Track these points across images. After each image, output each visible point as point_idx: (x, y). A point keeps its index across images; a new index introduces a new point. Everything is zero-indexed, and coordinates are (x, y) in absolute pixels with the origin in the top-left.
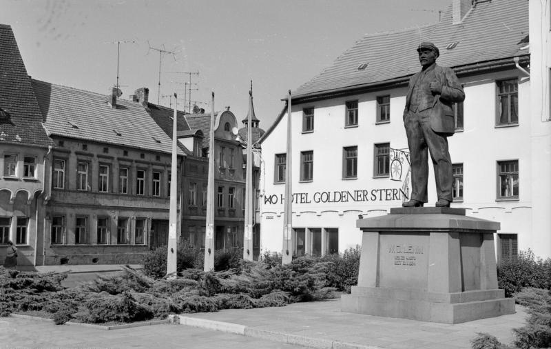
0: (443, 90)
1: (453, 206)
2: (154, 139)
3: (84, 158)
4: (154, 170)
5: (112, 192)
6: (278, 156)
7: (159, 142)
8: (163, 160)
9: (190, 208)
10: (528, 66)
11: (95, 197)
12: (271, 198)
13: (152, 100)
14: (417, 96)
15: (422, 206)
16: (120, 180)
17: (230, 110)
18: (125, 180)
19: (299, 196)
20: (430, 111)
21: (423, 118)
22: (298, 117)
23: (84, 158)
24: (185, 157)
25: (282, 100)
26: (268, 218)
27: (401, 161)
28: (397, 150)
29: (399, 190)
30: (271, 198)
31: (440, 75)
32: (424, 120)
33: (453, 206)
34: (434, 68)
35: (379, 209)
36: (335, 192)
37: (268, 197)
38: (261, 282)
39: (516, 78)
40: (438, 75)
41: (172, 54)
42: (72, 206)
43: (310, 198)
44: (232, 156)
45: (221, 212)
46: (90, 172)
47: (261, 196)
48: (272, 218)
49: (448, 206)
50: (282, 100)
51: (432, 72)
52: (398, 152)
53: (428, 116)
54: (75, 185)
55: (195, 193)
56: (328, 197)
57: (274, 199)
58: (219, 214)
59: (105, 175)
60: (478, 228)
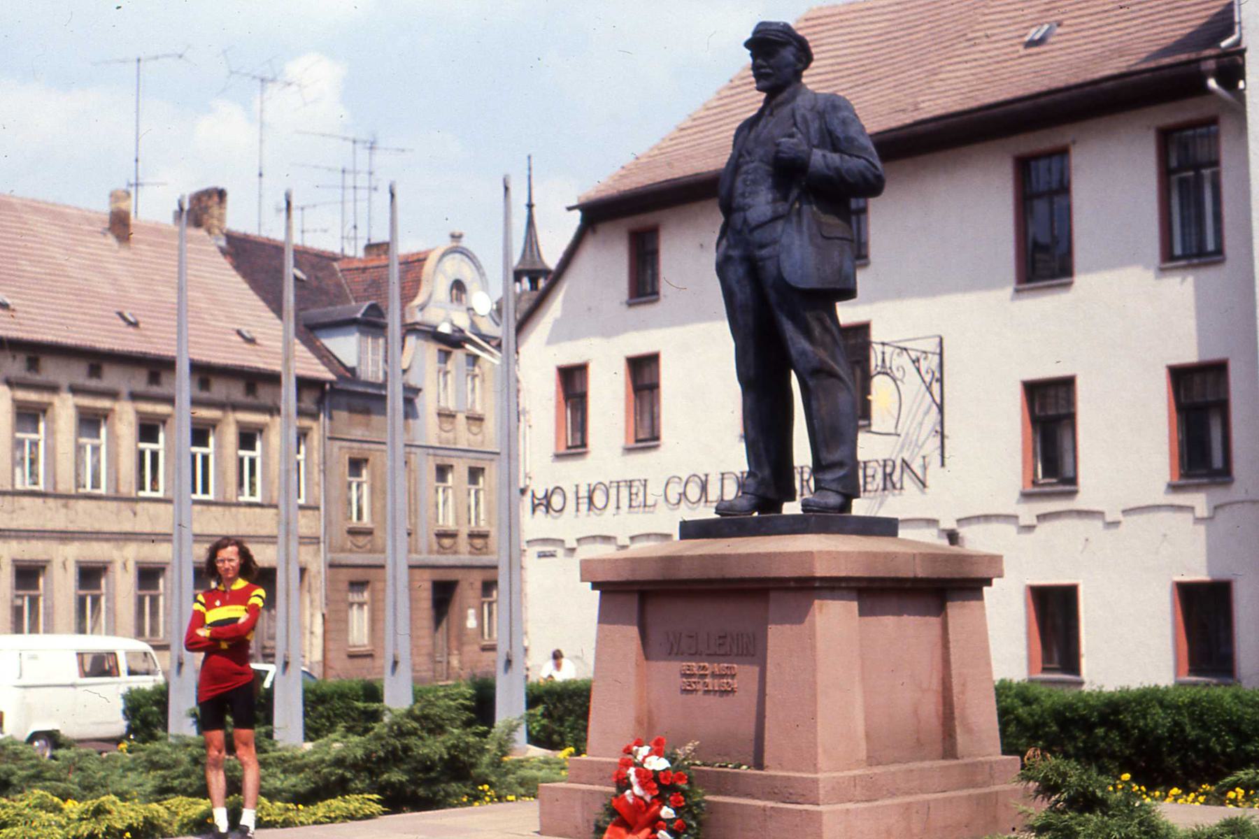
0: (813, 158)
1: (860, 508)
2: (239, 333)
3: (33, 396)
4: (238, 423)
5: (117, 490)
6: (1180, 376)
7: (251, 341)
8: (264, 394)
9: (353, 532)
10: (1241, 85)
11: (66, 506)
12: (548, 497)
13: (241, 217)
14: (745, 181)
15: (779, 510)
16: (79, 449)
17: (464, 243)
18: (252, 462)
19: (624, 492)
20: (779, 226)
21: (762, 246)
22: (608, 263)
23: (33, 396)
24: (331, 382)
25: (570, 209)
26: (542, 555)
27: (898, 375)
28: (883, 344)
29: (898, 463)
30: (548, 497)
31: (809, 116)
32: (764, 252)
33: (860, 508)
34: (793, 97)
35: (649, 527)
36: (723, 474)
37: (540, 494)
38: (1243, 727)
39: (1214, 121)
40: (804, 117)
41: (294, 88)
42: (65, 536)
43: (655, 490)
44: (446, 373)
45: (447, 542)
46: (51, 433)
47: (523, 491)
48: (552, 555)
49: (846, 506)
50: (570, 209)
51: (786, 110)
52: (888, 349)
53: (775, 242)
54: (73, 482)
55: (365, 488)
56: (704, 488)
57: (556, 501)
58: (441, 546)
59: (33, 436)
60: (920, 575)
